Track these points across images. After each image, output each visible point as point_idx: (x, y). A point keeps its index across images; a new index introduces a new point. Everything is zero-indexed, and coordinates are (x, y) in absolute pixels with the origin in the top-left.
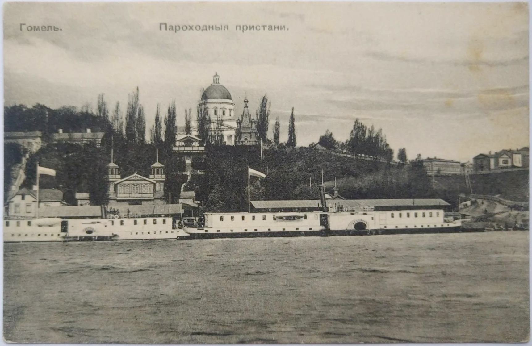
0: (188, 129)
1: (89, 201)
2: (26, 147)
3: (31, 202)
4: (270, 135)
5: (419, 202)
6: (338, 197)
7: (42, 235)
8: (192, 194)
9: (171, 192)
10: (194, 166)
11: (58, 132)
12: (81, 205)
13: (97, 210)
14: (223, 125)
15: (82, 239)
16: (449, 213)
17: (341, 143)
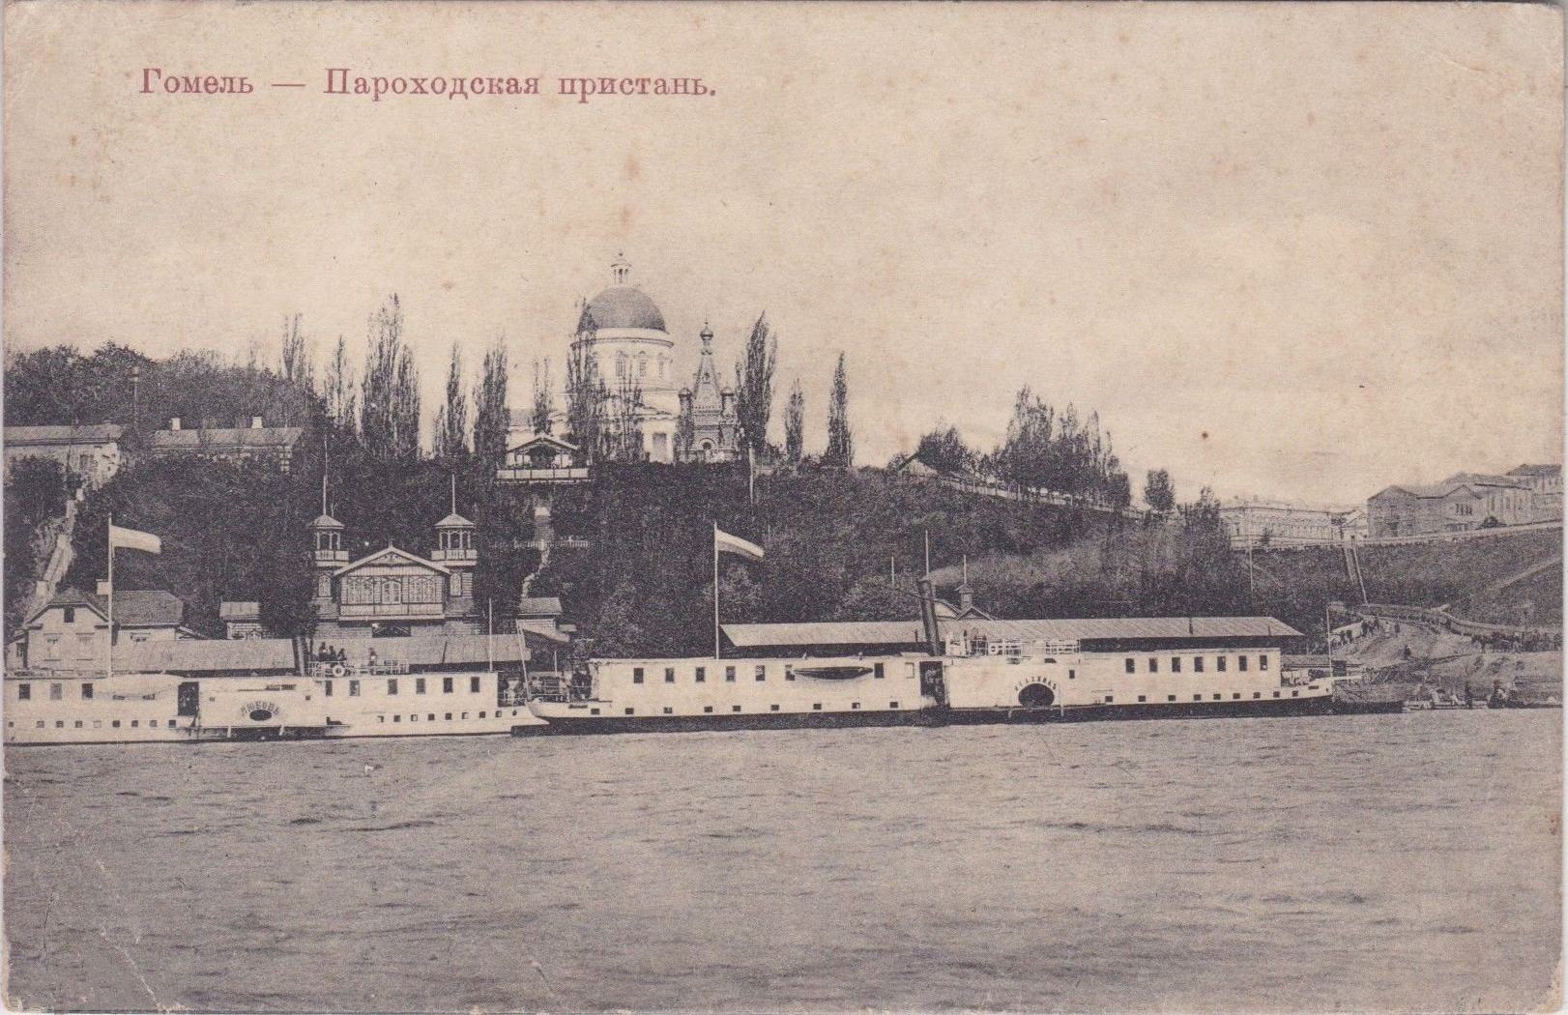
1: (258, 626)
4: (776, 433)
7: (144, 726)
10: (561, 524)
11: (167, 426)
12: (237, 637)
13: (281, 650)
15: (243, 735)
16: (1300, 658)
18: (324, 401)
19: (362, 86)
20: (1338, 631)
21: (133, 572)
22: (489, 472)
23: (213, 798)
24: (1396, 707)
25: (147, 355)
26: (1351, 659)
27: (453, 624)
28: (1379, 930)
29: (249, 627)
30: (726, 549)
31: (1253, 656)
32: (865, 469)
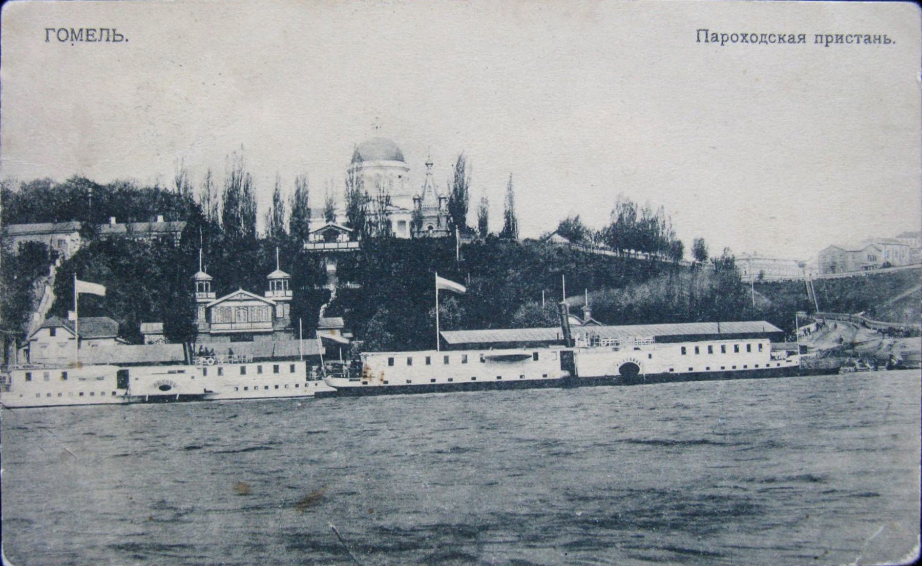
0: (329, 215)
1: (162, 337)
2: (56, 248)
3: (66, 340)
4: (472, 221)
5: (728, 327)
6: (591, 322)
7: (87, 395)
8: (340, 321)
9: (303, 320)
10: (342, 275)
11: (108, 222)
12: (150, 343)
13: (176, 350)
14: (391, 205)
15: (154, 399)
16: (779, 345)
17: (595, 232)
18: (200, 206)
19: (715, 38)
20: (802, 328)
21: (90, 307)
22: (299, 245)
23: (140, 436)
24: (835, 371)
25: (97, 182)
26: (810, 345)
27: (278, 333)
28: (826, 497)
29: (158, 337)
30: (442, 287)
31: (754, 343)
32: (526, 240)
